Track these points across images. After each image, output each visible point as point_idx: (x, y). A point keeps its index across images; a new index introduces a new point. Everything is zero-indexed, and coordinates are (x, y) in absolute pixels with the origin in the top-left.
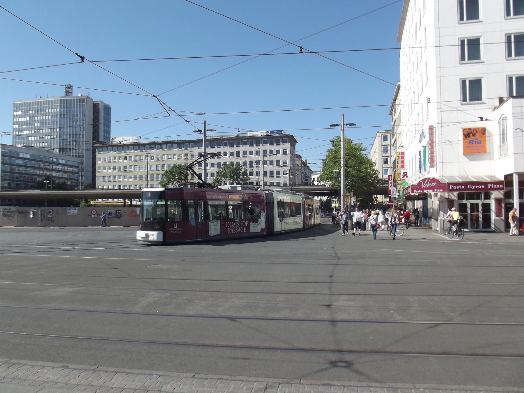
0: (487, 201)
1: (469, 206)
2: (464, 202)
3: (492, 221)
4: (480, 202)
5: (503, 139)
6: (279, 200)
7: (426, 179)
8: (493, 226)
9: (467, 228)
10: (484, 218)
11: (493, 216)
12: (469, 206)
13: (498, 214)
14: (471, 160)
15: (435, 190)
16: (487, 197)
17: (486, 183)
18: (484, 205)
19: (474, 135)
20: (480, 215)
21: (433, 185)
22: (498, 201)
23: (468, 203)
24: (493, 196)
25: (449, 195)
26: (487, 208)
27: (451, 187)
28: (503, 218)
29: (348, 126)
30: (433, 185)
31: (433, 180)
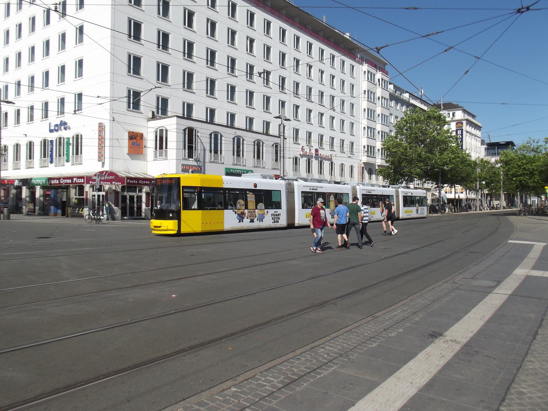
0: (140, 194)
1: (128, 197)
2: (125, 193)
3: (143, 210)
4: (135, 194)
5: (238, 152)
6: (365, 193)
7: (103, 172)
8: (143, 215)
9: (126, 216)
10: (137, 208)
11: (144, 206)
12: (128, 197)
13: (147, 205)
14: (132, 159)
15: (113, 183)
16: (140, 191)
17: (138, 179)
18: (138, 197)
19: (135, 138)
20: (135, 205)
21: (111, 178)
22: (147, 194)
23: (128, 194)
24: (144, 190)
25: (116, 188)
26: (139, 198)
27: (128, 181)
28: (150, 208)
29: (5, 103)
30: (111, 178)
31: (111, 174)
